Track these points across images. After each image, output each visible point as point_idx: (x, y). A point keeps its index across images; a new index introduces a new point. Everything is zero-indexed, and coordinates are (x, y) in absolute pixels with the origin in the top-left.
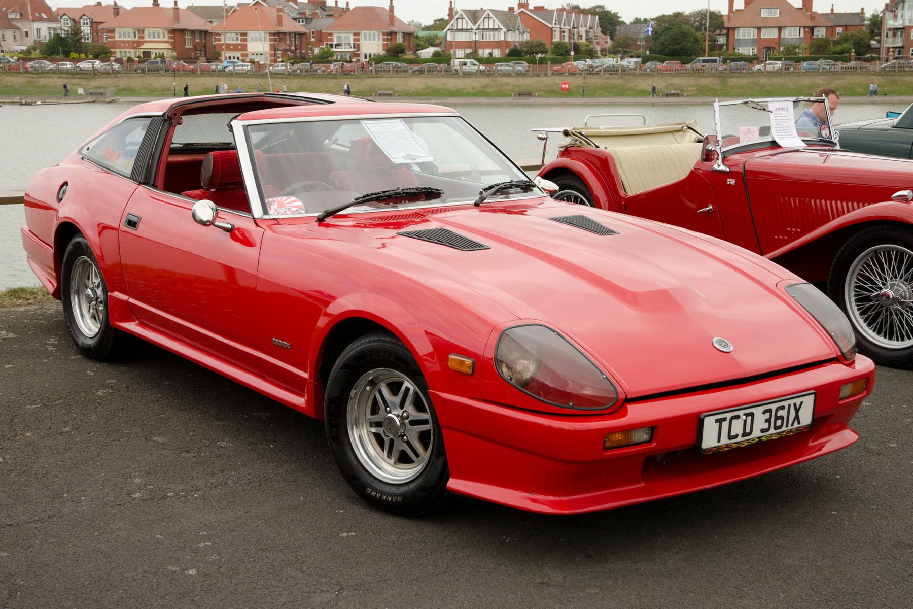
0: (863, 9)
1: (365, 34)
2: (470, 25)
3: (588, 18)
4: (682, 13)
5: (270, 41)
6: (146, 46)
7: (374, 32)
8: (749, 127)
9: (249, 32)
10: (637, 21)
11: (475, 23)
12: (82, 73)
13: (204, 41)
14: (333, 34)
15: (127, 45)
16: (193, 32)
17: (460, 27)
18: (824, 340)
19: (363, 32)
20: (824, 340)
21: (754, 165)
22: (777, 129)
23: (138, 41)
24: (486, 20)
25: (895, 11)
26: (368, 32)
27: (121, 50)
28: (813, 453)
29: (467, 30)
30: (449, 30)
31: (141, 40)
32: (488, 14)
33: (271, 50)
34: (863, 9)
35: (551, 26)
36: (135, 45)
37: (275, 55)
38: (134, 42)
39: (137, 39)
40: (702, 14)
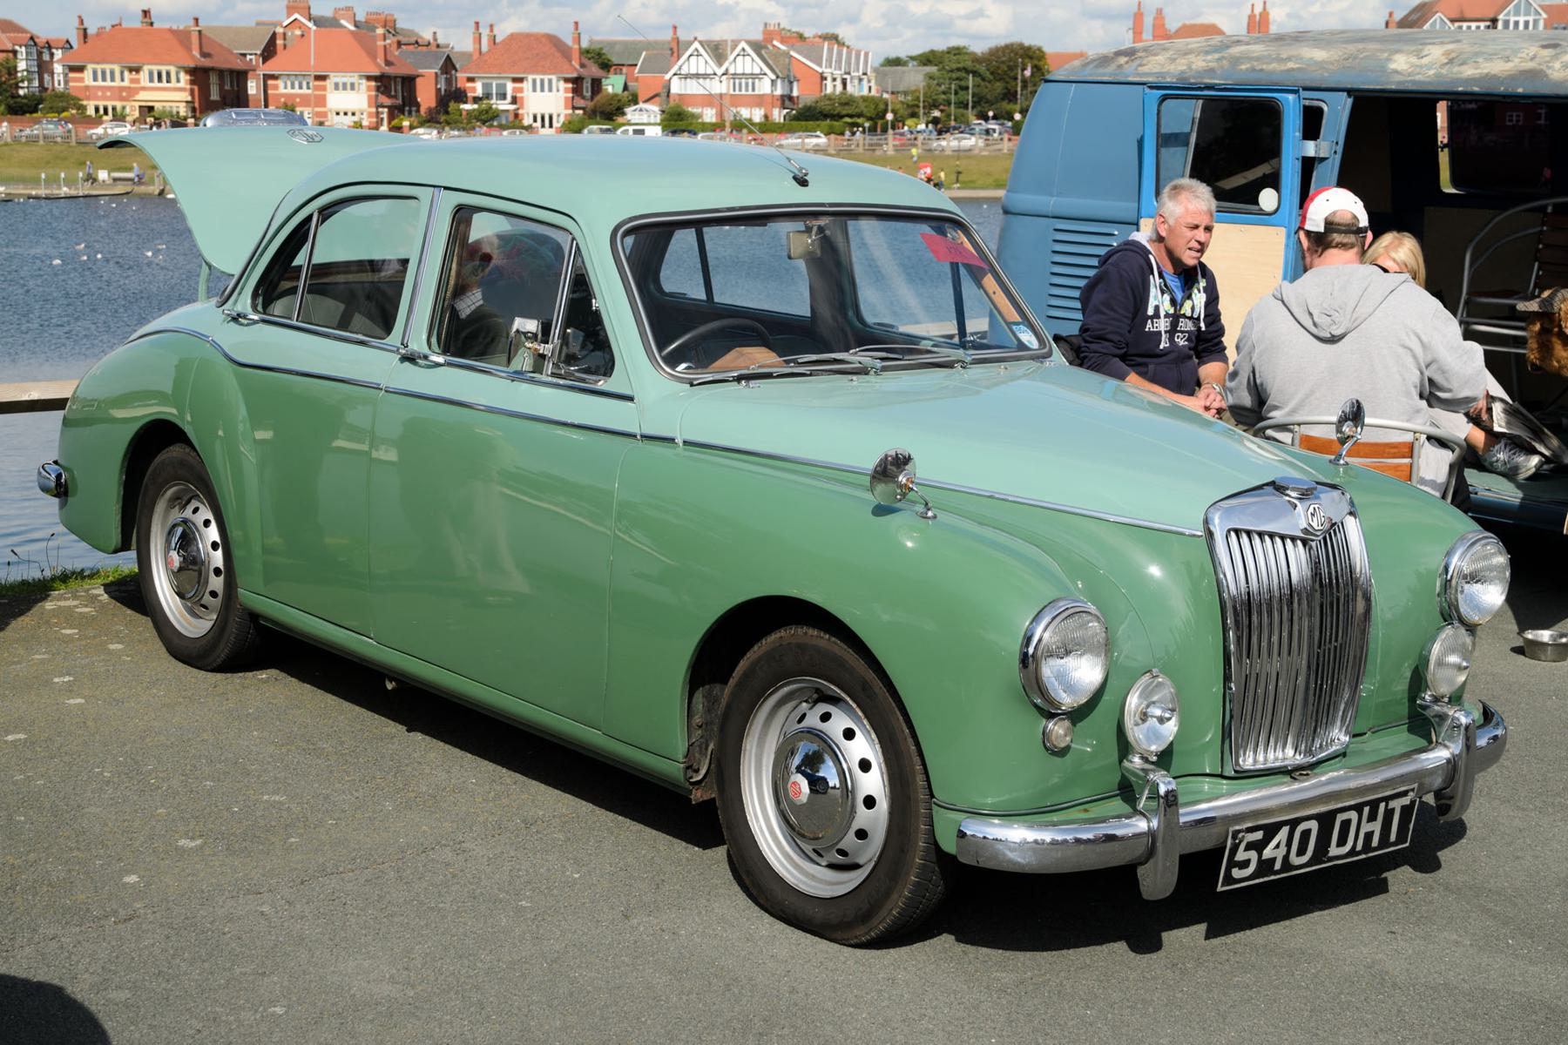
1: (534, 81)
2: (712, 67)
4: (964, 47)
5: (566, 92)
6: (143, 95)
7: (550, 77)
8: (875, 769)
9: (332, 74)
11: (720, 64)
13: (236, 88)
15: (109, 94)
16: (221, 73)
17: (693, 71)
19: (530, 77)
22: (1264, 607)
23: (130, 88)
24: (693, 59)
26: (538, 77)
27: (97, 103)
29: (705, 76)
30: (675, 74)
31: (133, 85)
33: (370, 106)
35: (820, 70)
36: (124, 94)
38: (121, 89)
39: (126, 83)
40: (1012, 51)
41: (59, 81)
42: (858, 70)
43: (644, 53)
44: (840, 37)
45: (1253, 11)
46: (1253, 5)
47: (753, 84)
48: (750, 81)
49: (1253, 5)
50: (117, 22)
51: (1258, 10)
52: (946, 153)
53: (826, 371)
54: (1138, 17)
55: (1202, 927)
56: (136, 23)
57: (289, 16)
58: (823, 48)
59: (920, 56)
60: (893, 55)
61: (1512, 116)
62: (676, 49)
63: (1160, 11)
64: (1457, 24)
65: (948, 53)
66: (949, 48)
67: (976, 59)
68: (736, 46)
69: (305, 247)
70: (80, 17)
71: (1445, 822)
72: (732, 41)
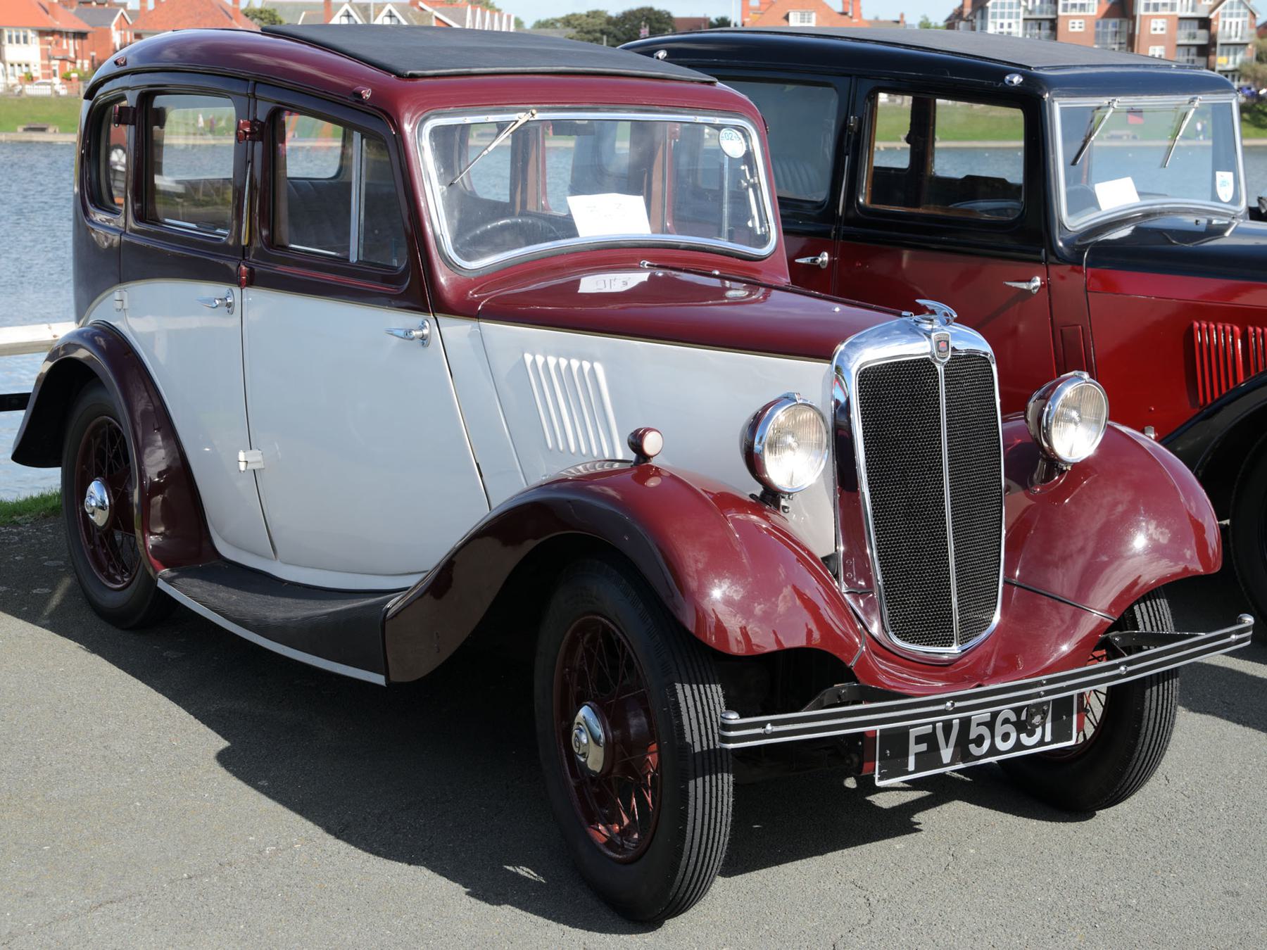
0: (902, 16)
3: (303, 20)
10: (541, 25)
12: (969, 653)
14: (143, 36)
18: (1191, 426)
20: (1194, 424)
21: (775, 209)
25: (972, 21)
28: (515, 288)
32: (390, 11)
33: (42, 58)
34: (902, 16)
37: (49, 67)
41: (1119, 138)
43: (304, 13)
46: (40, 4)
49: (40, 4)
50: (898, 18)
53: (800, 547)
55: (224, 744)
58: (466, 11)
59: (563, 18)
65: (588, 16)
66: (588, 12)
67: (610, 21)
68: (384, 7)
69: (1207, 662)
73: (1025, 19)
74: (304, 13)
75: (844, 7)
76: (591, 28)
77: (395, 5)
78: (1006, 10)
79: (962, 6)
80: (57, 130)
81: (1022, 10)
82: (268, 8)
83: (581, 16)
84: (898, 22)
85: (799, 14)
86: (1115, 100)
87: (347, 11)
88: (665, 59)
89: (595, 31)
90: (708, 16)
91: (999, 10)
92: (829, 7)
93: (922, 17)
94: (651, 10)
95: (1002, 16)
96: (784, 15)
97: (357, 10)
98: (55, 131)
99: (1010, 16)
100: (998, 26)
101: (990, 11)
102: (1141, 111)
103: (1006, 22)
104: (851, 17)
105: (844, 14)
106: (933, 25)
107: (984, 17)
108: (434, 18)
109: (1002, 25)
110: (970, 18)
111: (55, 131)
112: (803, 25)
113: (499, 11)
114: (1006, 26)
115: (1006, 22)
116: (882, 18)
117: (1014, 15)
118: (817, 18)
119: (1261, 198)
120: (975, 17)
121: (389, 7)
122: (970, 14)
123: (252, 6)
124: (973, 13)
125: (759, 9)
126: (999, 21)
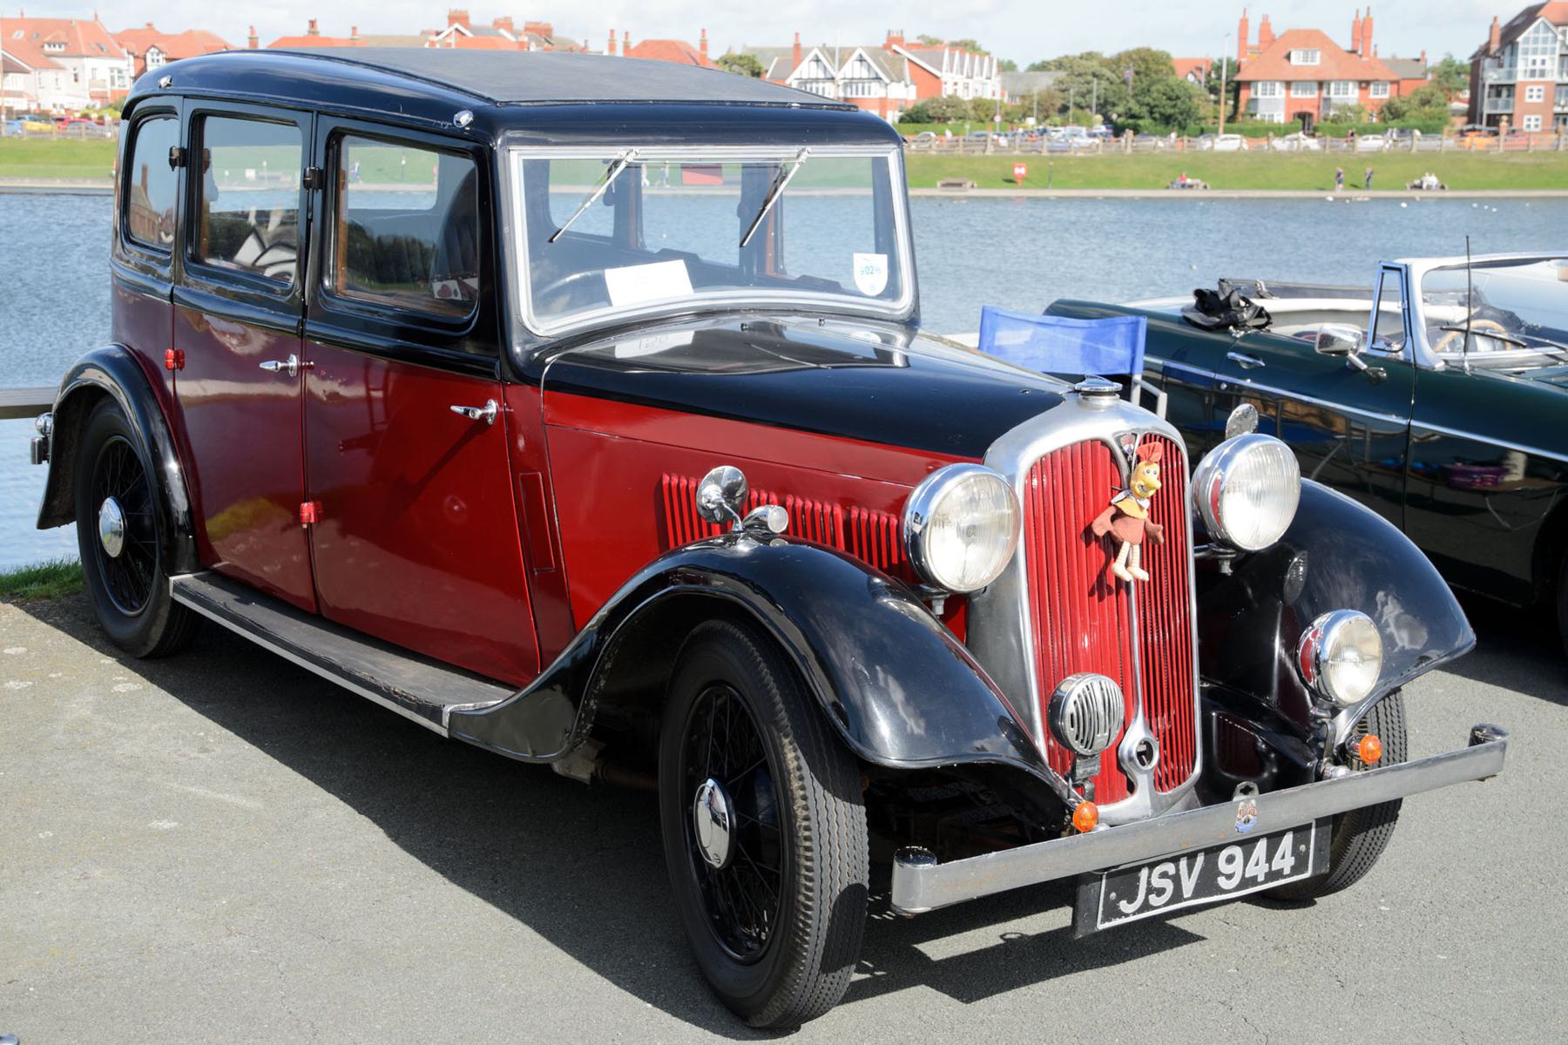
0: (1423, 54)
25: (1499, 58)
32: (861, 55)
34: (1423, 54)
42: (981, 74)
43: (776, 59)
44: (978, 44)
45: (1357, 16)
47: (869, 88)
48: (860, 86)
50: (1418, 56)
51: (1362, 15)
52: (25, 139)
54: (1244, 24)
56: (146, 27)
57: (450, 24)
58: (943, 54)
59: (1055, 61)
60: (1038, 61)
61: (1529, 120)
62: (798, 53)
63: (1266, 18)
64: (1560, 29)
65: (1081, 58)
70: (252, 27)
71: (876, 670)
72: (841, 49)
73: (1562, 55)
74: (776, 59)
75: (1353, 45)
76: (1082, 71)
77: (866, 49)
78: (1540, 46)
79: (1489, 43)
80: (976, 185)
81: (1558, 45)
82: (749, 54)
83: (1074, 58)
84: (1418, 60)
85: (1301, 53)
86: (803, 150)
87: (817, 56)
88: (458, 108)
89: (1086, 74)
90: (1211, 56)
91: (1531, 46)
92: (1336, 46)
93: (1446, 54)
94: (1148, 50)
95: (1535, 52)
96: (1285, 54)
97: (827, 55)
98: (973, 186)
99: (1544, 52)
100: (1530, 62)
101: (1521, 47)
102: (718, 167)
103: (1539, 58)
104: (1360, 56)
105: (1354, 52)
106: (1457, 63)
107: (1513, 53)
108: (906, 60)
109: (1534, 62)
110: (1498, 55)
111: (973, 186)
112: (1305, 64)
113: (988, 54)
114: (1539, 62)
115: (1539, 58)
116: (1400, 56)
117: (1549, 51)
118: (1321, 57)
119: (1222, 281)
120: (1503, 53)
121: (859, 51)
122: (1498, 50)
123: (732, 52)
124: (1502, 50)
125: (1259, 49)
126: (1531, 57)
